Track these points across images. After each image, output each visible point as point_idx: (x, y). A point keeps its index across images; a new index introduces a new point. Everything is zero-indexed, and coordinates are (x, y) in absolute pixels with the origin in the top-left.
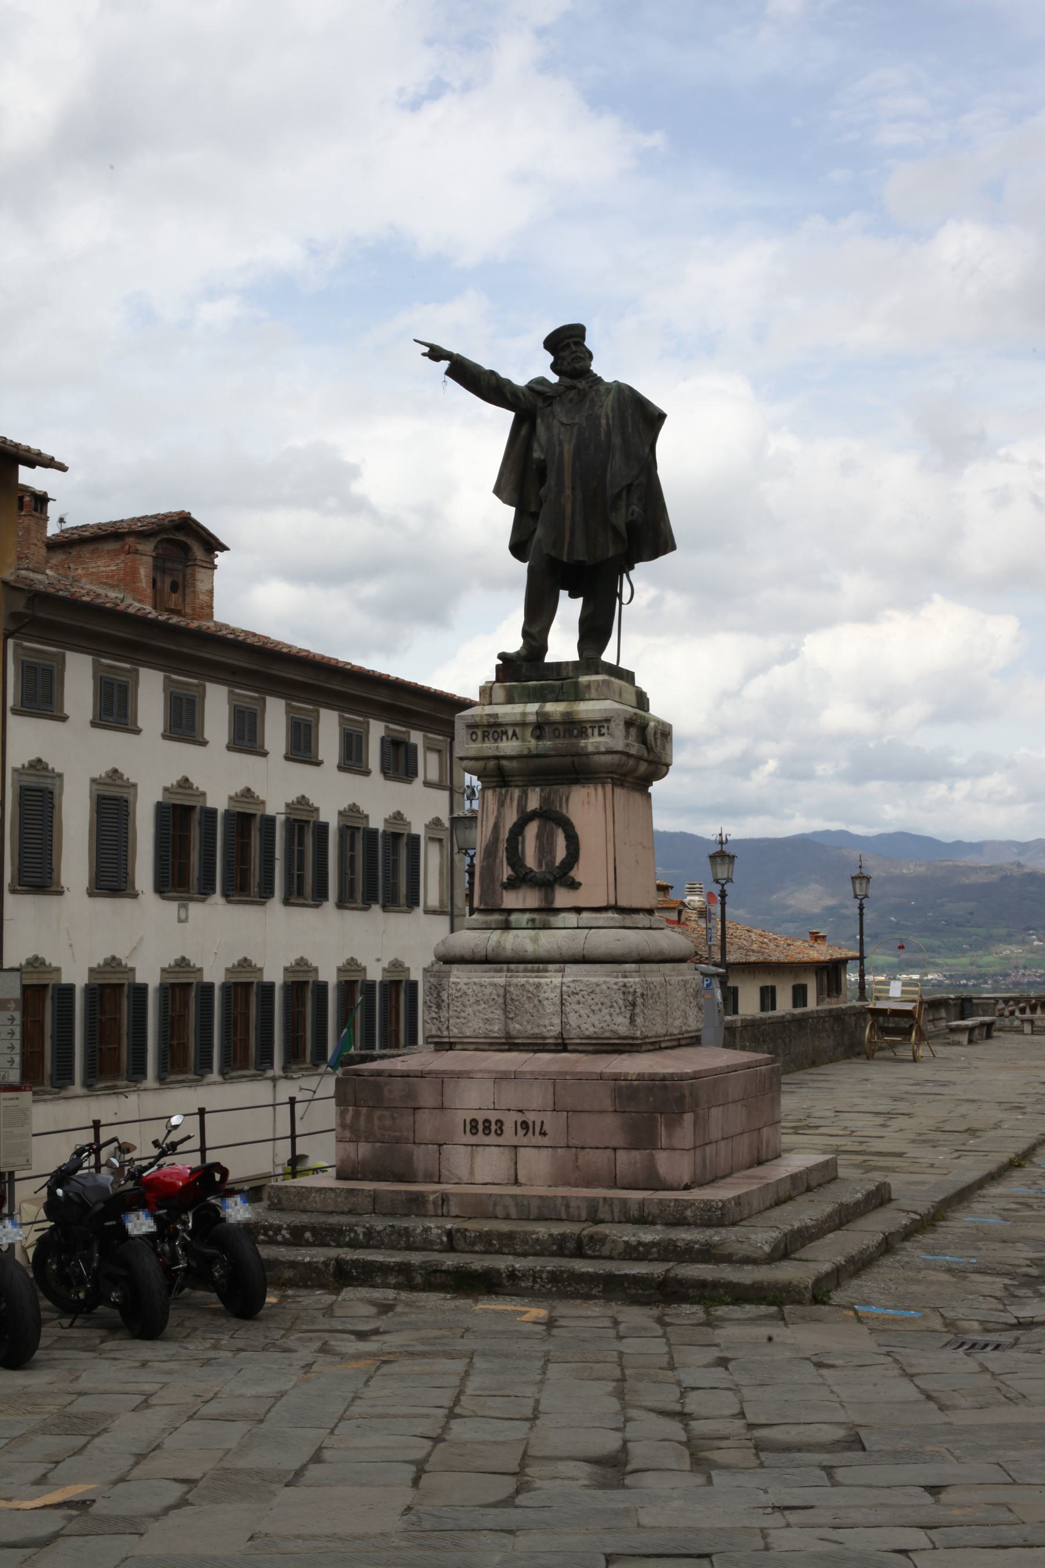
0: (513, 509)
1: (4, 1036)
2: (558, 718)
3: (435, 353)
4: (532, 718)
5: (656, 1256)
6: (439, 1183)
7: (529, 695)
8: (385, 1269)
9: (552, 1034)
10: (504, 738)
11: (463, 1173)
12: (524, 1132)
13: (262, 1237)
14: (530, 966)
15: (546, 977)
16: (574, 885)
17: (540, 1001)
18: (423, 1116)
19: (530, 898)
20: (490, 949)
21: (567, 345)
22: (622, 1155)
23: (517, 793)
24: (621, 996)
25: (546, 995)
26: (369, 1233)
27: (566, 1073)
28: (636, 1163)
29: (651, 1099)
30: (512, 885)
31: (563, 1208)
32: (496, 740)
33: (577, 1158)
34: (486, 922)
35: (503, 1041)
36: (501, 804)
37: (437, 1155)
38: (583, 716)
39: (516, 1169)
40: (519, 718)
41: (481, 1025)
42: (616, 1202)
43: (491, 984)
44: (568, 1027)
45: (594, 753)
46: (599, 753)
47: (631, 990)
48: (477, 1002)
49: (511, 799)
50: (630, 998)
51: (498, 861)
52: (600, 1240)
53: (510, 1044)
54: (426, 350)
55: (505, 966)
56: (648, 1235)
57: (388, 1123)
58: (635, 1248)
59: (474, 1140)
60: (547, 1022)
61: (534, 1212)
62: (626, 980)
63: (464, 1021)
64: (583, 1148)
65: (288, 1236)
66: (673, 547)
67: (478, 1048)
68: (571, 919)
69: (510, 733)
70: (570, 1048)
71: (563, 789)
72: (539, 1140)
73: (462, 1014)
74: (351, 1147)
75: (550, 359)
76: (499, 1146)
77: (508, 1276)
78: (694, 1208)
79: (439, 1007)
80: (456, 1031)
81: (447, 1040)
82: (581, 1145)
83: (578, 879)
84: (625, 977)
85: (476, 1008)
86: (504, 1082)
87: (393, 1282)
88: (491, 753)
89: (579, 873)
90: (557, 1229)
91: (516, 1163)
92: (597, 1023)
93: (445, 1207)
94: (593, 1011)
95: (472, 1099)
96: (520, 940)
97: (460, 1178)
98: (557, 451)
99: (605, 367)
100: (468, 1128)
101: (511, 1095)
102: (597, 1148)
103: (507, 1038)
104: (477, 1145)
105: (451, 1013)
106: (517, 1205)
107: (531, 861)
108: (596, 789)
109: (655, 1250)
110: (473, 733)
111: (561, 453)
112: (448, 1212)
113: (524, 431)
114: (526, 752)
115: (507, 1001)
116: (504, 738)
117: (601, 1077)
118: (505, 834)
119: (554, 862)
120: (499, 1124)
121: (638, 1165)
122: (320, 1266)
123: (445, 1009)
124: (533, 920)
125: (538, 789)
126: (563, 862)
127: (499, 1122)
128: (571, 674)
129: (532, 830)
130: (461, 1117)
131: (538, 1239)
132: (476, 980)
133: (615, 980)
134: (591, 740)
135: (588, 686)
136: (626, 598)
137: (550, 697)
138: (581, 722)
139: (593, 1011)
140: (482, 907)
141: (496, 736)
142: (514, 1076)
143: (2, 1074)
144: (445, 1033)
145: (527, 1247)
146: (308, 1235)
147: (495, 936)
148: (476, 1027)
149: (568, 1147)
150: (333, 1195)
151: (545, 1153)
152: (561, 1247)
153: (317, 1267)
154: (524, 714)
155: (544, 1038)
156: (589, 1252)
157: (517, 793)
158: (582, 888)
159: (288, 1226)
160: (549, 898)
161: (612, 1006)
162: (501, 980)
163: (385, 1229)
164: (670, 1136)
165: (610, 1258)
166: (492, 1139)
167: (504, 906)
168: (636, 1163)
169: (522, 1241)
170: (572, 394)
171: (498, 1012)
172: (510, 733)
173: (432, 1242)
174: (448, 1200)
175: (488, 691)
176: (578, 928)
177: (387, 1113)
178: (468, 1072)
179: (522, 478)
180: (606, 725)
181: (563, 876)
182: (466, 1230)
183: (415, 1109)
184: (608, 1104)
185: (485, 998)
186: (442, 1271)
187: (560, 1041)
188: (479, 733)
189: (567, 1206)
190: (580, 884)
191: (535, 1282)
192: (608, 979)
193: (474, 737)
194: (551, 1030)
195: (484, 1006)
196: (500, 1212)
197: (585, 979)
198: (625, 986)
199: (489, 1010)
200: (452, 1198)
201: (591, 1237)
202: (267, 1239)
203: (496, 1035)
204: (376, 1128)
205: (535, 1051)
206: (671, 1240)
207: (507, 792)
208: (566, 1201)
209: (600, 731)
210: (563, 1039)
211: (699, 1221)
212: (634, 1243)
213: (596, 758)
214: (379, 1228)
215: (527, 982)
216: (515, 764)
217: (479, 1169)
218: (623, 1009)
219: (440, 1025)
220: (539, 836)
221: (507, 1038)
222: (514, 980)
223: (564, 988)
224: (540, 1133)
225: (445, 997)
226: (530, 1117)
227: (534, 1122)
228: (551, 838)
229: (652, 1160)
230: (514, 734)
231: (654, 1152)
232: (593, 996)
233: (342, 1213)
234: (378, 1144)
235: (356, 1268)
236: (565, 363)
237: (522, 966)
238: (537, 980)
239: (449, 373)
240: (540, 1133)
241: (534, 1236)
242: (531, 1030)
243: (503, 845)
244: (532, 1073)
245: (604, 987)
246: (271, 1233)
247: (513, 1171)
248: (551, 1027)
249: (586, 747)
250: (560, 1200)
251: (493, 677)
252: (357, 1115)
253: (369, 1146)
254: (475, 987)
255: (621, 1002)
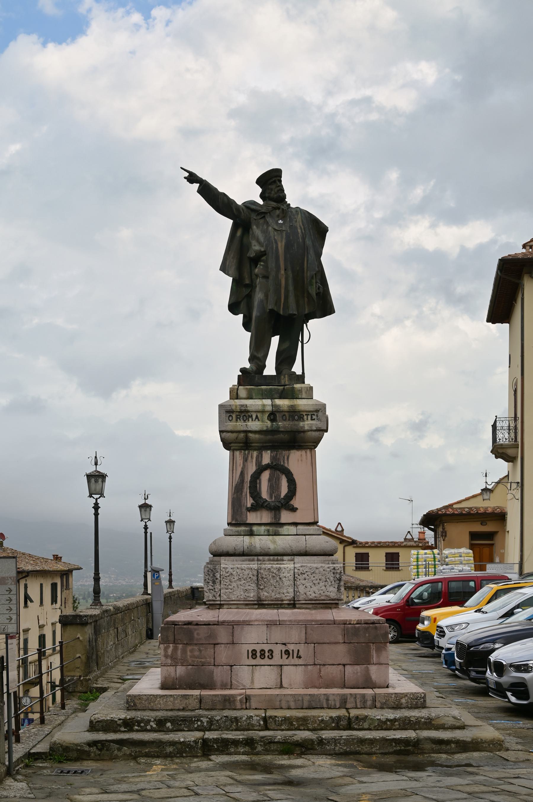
0: (230, 279)
1: (3, 602)
2: (286, 408)
3: (192, 178)
4: (269, 408)
5: (398, 726)
6: (231, 688)
7: (262, 395)
8: (236, 743)
9: (288, 598)
10: (250, 419)
11: (247, 682)
12: (287, 656)
13: (136, 727)
14: (272, 557)
15: (284, 564)
16: (294, 510)
17: (280, 578)
18: (220, 649)
19: (265, 517)
20: (246, 547)
21: (270, 181)
22: (348, 669)
23: (255, 454)
24: (332, 575)
25: (284, 575)
26: (211, 721)
27: (312, 621)
28: (357, 673)
29: (367, 635)
30: (254, 508)
31: (325, 701)
32: (245, 421)
33: (320, 671)
34: (238, 531)
35: (256, 602)
36: (245, 460)
37: (230, 672)
38: (302, 408)
39: (281, 679)
40: (260, 408)
41: (242, 593)
42: (358, 696)
43: (248, 569)
44: (298, 594)
45: (308, 431)
46: (311, 431)
47: (339, 571)
48: (239, 579)
49: (252, 457)
50: (338, 576)
51: (244, 494)
52: (362, 719)
53: (260, 604)
54: (187, 174)
55: (256, 558)
56: (391, 715)
57: (197, 653)
58: (385, 723)
59: (254, 662)
60: (285, 591)
61: (306, 704)
62: (335, 565)
63: (231, 591)
64: (324, 665)
65: (154, 726)
66: (334, 312)
67: (238, 606)
68: (292, 530)
69: (254, 417)
70: (297, 606)
71: (285, 453)
72: (296, 661)
73: (230, 587)
74: (172, 669)
75: (259, 190)
76: (270, 665)
77: (318, 743)
78: (406, 698)
79: (214, 582)
80: (225, 597)
81: (219, 602)
82: (322, 663)
83: (295, 506)
84: (334, 564)
85: (239, 583)
86: (273, 627)
87: (242, 751)
88: (242, 429)
89: (295, 502)
90: (334, 713)
91: (281, 675)
92: (317, 591)
93: (247, 704)
94: (314, 584)
95: (253, 638)
96: (262, 542)
97: (244, 686)
98: (274, 246)
99: (294, 196)
100: (250, 655)
101: (278, 635)
102: (333, 665)
103: (257, 601)
104: (256, 665)
105: (222, 586)
106: (295, 701)
107: (265, 495)
108: (306, 452)
109: (397, 723)
110: (230, 416)
111: (277, 247)
112: (250, 706)
113: (239, 233)
114: (265, 429)
115: (259, 578)
116: (250, 419)
117: (334, 622)
118: (248, 478)
119: (280, 496)
120: (270, 652)
121: (359, 674)
122: (192, 743)
123: (218, 584)
124: (268, 531)
125: (269, 452)
126: (286, 496)
127: (271, 651)
128: (287, 383)
129: (265, 476)
130: (245, 648)
131: (323, 720)
132: (239, 566)
133: (328, 565)
134: (306, 423)
135: (300, 391)
136: (306, 339)
137: (276, 396)
138: (299, 412)
139: (314, 584)
140: (234, 522)
141: (245, 418)
142: (279, 623)
143: (3, 627)
144: (218, 598)
145: (316, 725)
146: (169, 724)
147: (247, 539)
148: (238, 594)
149: (315, 664)
150: (172, 699)
151: (301, 668)
152: (337, 724)
153: (190, 744)
154: (264, 405)
155: (282, 600)
156: (356, 727)
157: (255, 454)
158: (298, 511)
159: (155, 720)
160: (277, 516)
161: (326, 581)
162: (254, 566)
163: (221, 718)
164: (378, 657)
165: (369, 729)
166: (266, 661)
167: (248, 522)
168: (357, 673)
169: (313, 722)
170: (278, 212)
171: (253, 585)
172: (254, 417)
173: (253, 725)
174: (250, 699)
175: (236, 391)
176: (297, 535)
177: (196, 648)
178: (250, 621)
179: (241, 261)
180: (315, 414)
181: (286, 504)
182: (276, 717)
183: (215, 644)
184: (340, 639)
185: (245, 577)
186: (274, 742)
187: (292, 602)
188: (234, 416)
189: (328, 700)
190: (297, 509)
191: (336, 745)
192: (323, 565)
193: (230, 418)
194: (287, 596)
195: (244, 581)
196: (284, 705)
197: (309, 565)
198: (334, 569)
199: (247, 584)
200: (252, 698)
201: (357, 717)
202: (140, 728)
203: (252, 599)
204: (189, 657)
205: (278, 608)
206: (406, 717)
207: (249, 453)
208: (327, 697)
209: (312, 417)
210: (294, 600)
211: (410, 706)
212: (384, 720)
213: (309, 433)
214: (218, 718)
215: (272, 567)
216: (257, 436)
217: (257, 680)
218: (333, 582)
219: (215, 594)
220: (270, 480)
221: (257, 601)
222: (263, 566)
223: (296, 571)
224: (297, 657)
225: (218, 577)
226: (291, 647)
227: (293, 650)
228: (278, 480)
229: (367, 670)
230: (257, 417)
231: (369, 666)
232: (314, 575)
233: (179, 710)
234: (190, 667)
235: (216, 743)
236: (273, 192)
237: (266, 558)
238: (278, 566)
239: (200, 191)
240: (297, 657)
241: (320, 719)
242: (274, 595)
243: (247, 485)
244: (290, 621)
245: (321, 570)
246: (142, 725)
247: (279, 680)
248: (288, 594)
249: (304, 427)
250: (323, 696)
251: (236, 383)
252: (175, 649)
253: (184, 668)
254: (238, 570)
255: (332, 578)
